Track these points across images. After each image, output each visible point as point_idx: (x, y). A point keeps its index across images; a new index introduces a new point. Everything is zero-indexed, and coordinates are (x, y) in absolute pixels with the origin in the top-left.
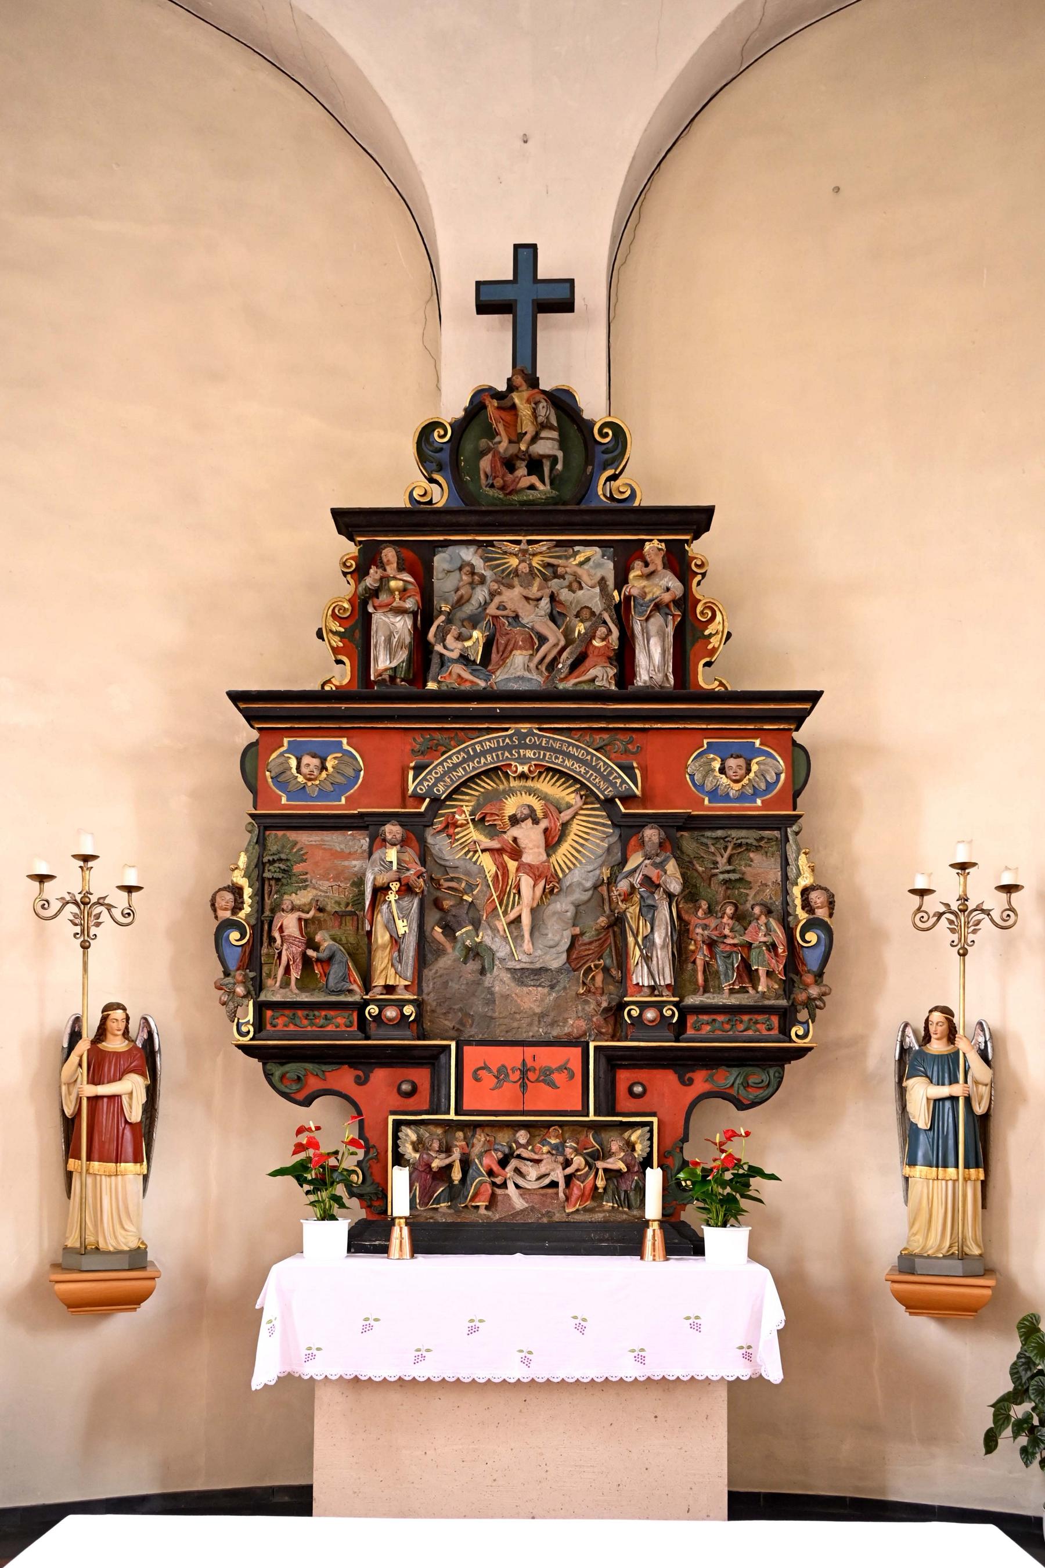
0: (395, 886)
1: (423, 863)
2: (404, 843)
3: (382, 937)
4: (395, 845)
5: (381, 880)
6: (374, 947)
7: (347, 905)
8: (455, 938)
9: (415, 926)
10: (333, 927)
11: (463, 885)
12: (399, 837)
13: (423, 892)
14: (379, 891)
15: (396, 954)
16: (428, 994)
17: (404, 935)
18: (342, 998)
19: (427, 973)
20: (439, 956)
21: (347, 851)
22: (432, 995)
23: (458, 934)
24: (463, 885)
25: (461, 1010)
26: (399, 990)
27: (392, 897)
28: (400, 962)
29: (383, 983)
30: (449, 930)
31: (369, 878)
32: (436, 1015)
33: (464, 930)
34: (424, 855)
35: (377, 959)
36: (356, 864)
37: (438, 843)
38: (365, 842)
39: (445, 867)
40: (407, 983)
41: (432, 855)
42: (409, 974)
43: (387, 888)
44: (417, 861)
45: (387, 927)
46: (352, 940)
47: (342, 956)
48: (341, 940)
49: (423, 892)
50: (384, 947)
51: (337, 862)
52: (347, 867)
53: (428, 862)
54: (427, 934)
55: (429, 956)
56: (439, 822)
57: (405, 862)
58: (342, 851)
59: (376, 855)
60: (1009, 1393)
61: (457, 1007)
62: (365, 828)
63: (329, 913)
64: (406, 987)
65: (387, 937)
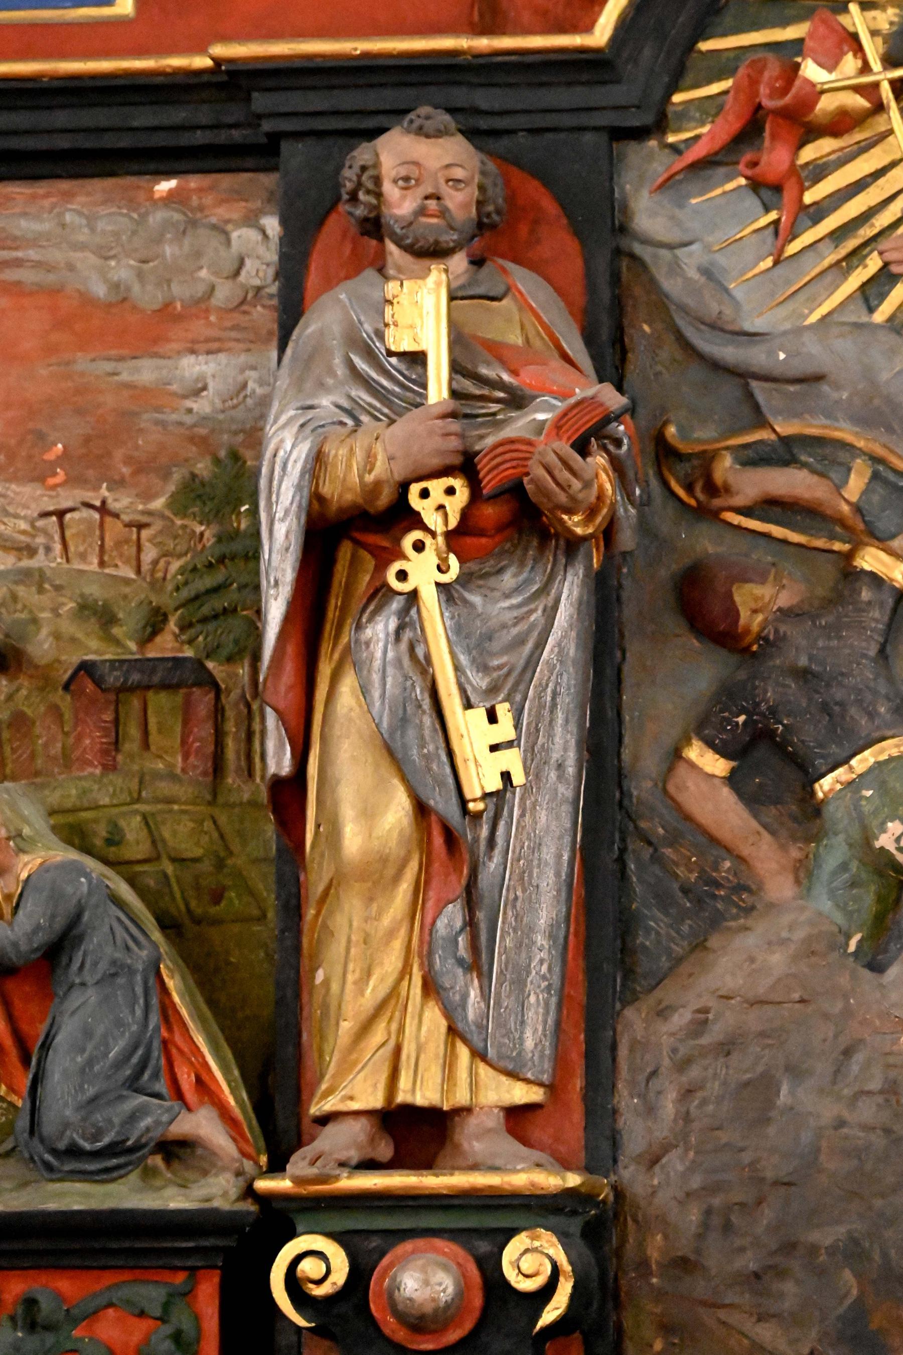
0: (440, 504)
1: (611, 355)
2: (489, 239)
3: (369, 814)
4: (435, 252)
5: (363, 464)
6: (317, 879)
7: (155, 623)
8: (812, 810)
9: (564, 743)
10: (67, 761)
11: (856, 485)
12: (460, 202)
13: (609, 533)
14: (352, 534)
15: (452, 916)
16: (653, 1161)
17: (497, 799)
18: (127, 1195)
19: (651, 1031)
20: (716, 922)
21: (148, 297)
22: (675, 1162)
23: (826, 785)
24: (856, 485)
25: (853, 1252)
26: (479, 1137)
27: (423, 569)
28: (477, 964)
29: (375, 1100)
30: (776, 763)
31: (287, 452)
32: (700, 1288)
33: (862, 762)
34: (616, 312)
35: (335, 950)
36: (205, 375)
37: (702, 235)
38: (256, 242)
39: (742, 376)
40: (521, 1094)
41: (661, 305)
42: (534, 1036)
43: (386, 519)
44: (576, 347)
45: (393, 755)
46: (181, 835)
47: (124, 934)
48: (115, 839)
49: (609, 533)
50: (377, 875)
51: (91, 366)
52: (143, 395)
53: (638, 362)
54: (641, 789)
55: (656, 929)
56: (702, 110)
57: (497, 351)
58: (121, 300)
59: (325, 319)
60: (631, 219)
61: (826, 1236)
62: (261, 154)
63: (44, 678)
64: (517, 1117)
65: (397, 811)
